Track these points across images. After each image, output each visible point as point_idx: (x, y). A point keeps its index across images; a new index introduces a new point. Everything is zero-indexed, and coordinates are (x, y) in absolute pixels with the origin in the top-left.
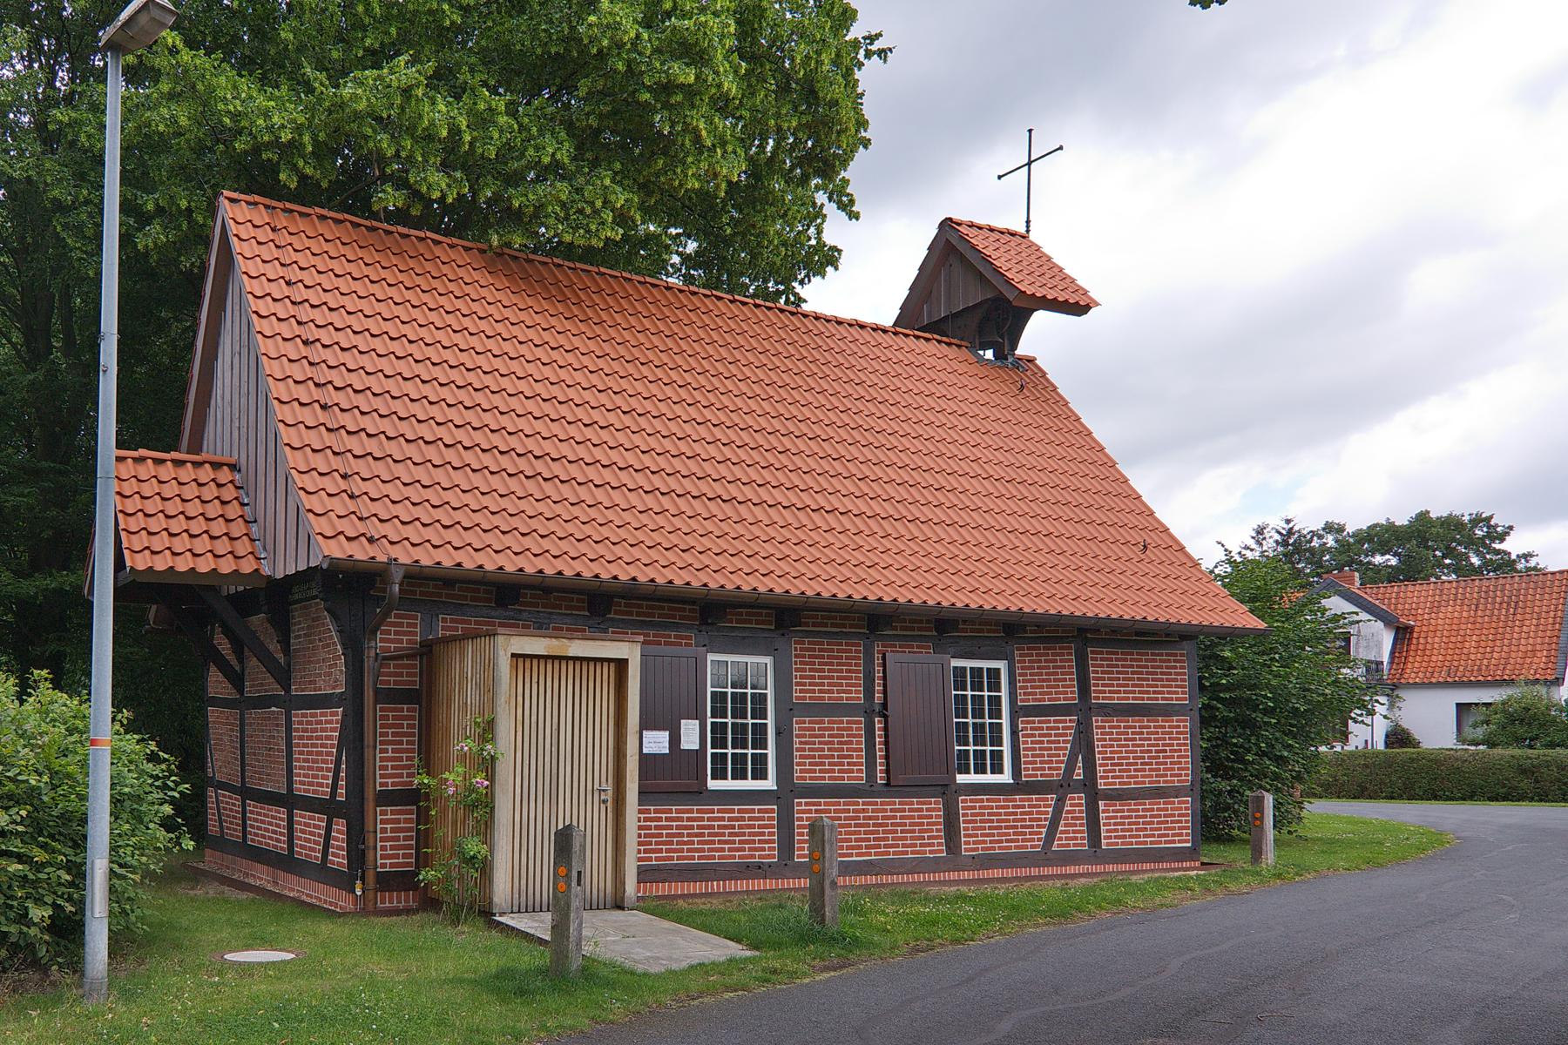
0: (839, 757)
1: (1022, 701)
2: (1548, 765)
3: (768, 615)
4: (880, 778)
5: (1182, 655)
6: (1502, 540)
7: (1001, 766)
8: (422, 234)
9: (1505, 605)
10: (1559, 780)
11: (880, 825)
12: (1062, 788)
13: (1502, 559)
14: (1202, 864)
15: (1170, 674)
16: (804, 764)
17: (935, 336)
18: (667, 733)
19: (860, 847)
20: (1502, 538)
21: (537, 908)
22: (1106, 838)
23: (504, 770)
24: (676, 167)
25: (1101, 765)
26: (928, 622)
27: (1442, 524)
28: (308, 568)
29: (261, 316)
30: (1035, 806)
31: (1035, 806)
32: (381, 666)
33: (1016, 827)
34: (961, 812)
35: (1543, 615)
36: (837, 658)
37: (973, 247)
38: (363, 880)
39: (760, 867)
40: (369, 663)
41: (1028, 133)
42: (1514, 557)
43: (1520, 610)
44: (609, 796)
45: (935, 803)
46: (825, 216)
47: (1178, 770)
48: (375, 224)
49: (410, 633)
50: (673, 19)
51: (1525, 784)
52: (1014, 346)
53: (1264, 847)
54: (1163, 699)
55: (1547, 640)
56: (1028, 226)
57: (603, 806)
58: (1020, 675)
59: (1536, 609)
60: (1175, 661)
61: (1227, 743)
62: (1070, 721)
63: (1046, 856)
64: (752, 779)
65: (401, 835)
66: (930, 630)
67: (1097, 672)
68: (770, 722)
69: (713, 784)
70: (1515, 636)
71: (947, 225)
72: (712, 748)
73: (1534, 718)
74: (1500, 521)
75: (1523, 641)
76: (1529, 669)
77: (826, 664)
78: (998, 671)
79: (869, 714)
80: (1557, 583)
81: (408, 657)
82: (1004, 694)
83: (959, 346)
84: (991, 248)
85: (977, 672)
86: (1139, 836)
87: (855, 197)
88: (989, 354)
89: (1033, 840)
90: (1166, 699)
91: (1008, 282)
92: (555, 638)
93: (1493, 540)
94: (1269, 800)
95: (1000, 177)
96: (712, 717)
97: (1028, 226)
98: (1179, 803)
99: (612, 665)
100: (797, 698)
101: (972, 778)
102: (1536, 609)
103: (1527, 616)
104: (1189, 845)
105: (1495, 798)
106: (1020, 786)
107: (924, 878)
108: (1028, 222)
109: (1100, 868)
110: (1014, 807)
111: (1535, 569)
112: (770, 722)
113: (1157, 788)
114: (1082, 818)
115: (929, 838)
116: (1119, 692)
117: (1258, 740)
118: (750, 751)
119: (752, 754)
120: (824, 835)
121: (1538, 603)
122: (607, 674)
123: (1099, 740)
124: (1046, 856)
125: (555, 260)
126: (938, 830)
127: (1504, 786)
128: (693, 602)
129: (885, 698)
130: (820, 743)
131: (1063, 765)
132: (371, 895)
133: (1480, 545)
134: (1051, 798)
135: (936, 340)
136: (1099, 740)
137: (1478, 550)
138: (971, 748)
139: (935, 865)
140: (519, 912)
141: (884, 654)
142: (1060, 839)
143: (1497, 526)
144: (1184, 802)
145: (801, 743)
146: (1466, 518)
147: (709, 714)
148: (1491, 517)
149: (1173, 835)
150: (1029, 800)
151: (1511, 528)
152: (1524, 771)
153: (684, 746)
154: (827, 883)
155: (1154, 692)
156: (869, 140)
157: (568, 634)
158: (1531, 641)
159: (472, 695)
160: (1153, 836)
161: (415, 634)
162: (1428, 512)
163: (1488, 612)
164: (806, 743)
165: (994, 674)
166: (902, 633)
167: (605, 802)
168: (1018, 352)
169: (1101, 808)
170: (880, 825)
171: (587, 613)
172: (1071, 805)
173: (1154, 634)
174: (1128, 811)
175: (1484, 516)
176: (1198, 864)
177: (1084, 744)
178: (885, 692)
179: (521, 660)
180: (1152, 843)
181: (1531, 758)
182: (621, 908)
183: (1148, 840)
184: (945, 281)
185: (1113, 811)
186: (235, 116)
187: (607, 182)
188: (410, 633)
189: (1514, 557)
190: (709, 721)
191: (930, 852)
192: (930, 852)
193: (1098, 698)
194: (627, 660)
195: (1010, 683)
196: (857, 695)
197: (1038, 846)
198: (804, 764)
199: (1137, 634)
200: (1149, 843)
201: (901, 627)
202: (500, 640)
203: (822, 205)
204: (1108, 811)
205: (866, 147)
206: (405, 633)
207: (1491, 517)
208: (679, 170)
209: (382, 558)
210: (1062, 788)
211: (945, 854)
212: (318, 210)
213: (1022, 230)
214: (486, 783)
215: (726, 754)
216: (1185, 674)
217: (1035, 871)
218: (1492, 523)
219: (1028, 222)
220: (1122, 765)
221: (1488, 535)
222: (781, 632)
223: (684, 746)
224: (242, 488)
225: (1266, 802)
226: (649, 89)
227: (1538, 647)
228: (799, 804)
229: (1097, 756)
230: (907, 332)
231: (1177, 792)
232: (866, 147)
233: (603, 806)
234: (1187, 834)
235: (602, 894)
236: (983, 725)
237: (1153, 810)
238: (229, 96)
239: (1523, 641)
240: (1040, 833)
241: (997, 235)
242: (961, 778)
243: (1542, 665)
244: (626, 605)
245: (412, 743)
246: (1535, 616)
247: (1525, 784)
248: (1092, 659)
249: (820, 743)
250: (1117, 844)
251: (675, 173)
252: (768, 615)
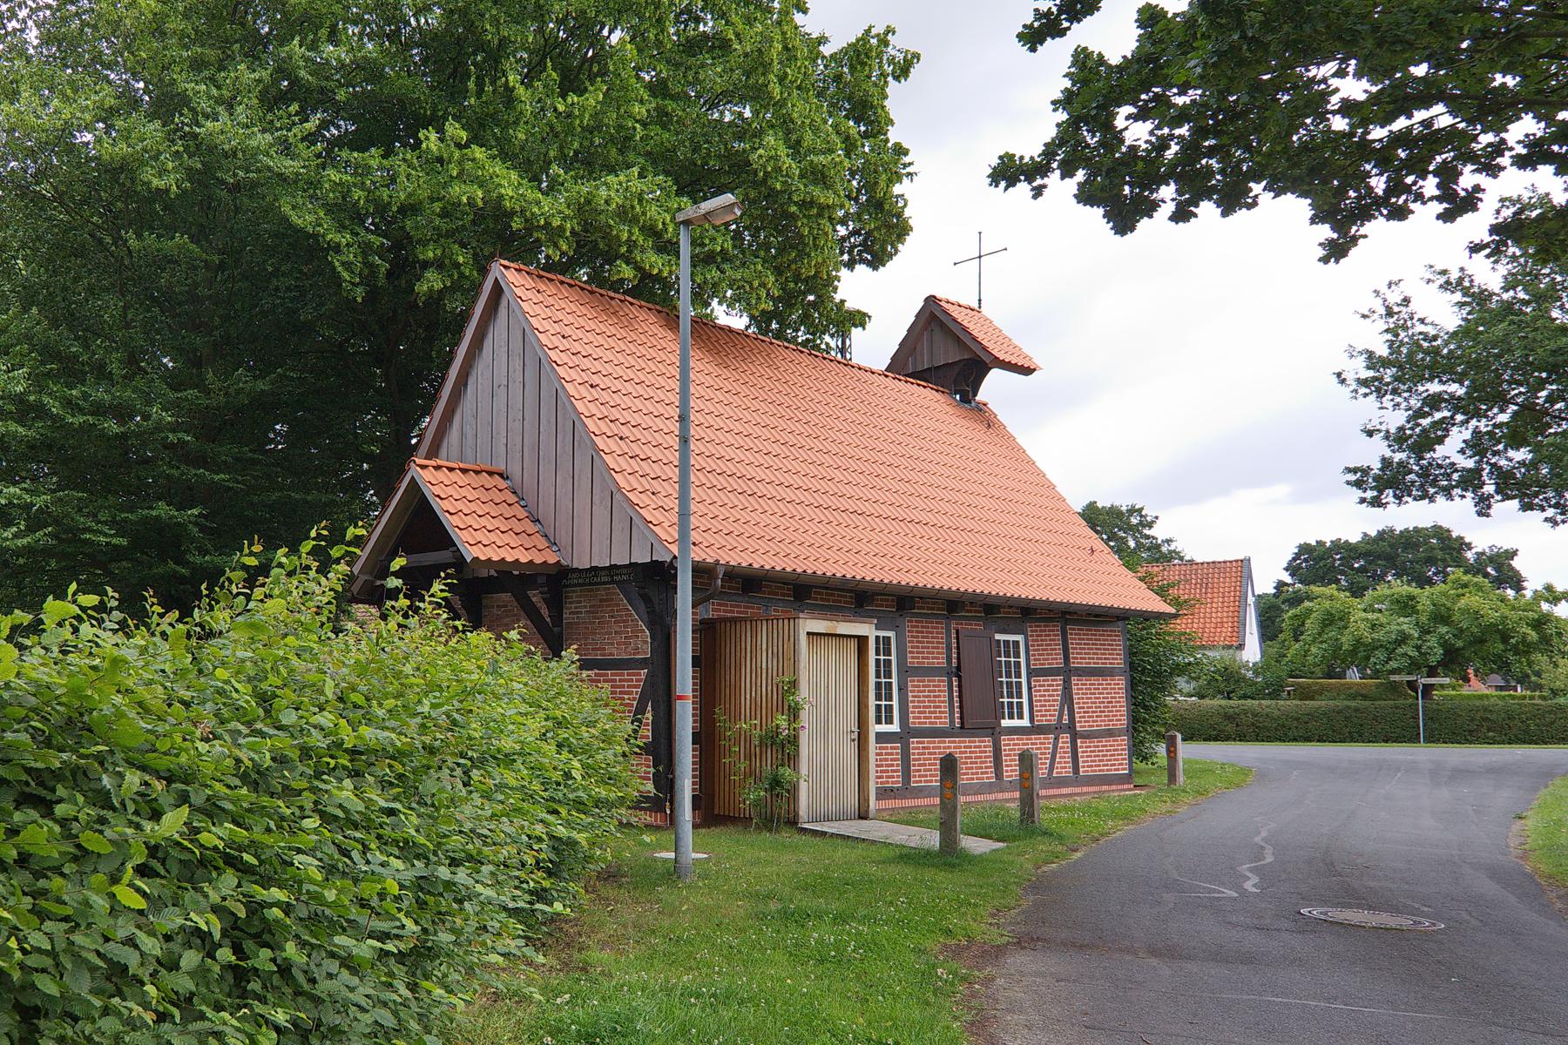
2: (1245, 712)
6: (1151, 527)
10: (1253, 724)
20: (1150, 525)
29: (558, 365)
42: (1159, 542)
43: (1209, 590)
44: (855, 736)
52: (975, 394)
55: (1230, 614)
56: (980, 304)
59: (1221, 590)
62: (1059, 680)
68: (894, 680)
74: (1149, 512)
75: (1214, 615)
76: (1220, 636)
83: (943, 392)
88: (958, 397)
97: (980, 304)
103: (1215, 595)
104: (1127, 772)
105: (1207, 739)
108: (980, 300)
111: (1174, 551)
113: (1109, 730)
121: (1222, 585)
122: (853, 645)
126: (990, 762)
146: (1124, 509)
148: (1142, 509)
151: (1157, 517)
152: (1229, 718)
158: (1219, 615)
162: (1095, 502)
163: (1187, 591)
167: (854, 740)
175: (1137, 507)
176: (1132, 786)
178: (958, 658)
182: (865, 818)
187: (759, 267)
189: (1159, 542)
196: (941, 661)
199: (1096, 616)
207: (1142, 509)
210: (1057, 729)
213: (976, 306)
218: (1143, 513)
219: (980, 300)
221: (1141, 523)
226: (796, 203)
227: (1225, 620)
230: (650, 306)
231: (1110, 733)
239: (1214, 615)
243: (1229, 634)
251: (803, 263)
252: (893, 601)
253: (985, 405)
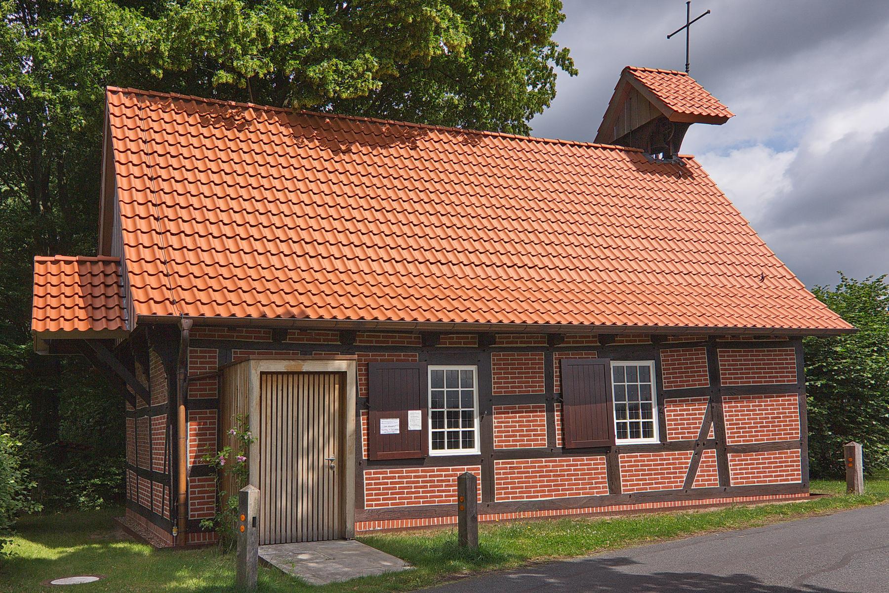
0: (527, 431)
4: (558, 444)
8: (402, 124)
11: (559, 476)
12: (699, 445)
14: (811, 495)
15: (783, 364)
16: (501, 437)
17: (618, 147)
18: (398, 420)
19: (544, 491)
21: (283, 540)
22: (733, 479)
23: (254, 449)
25: (728, 429)
26: (594, 337)
30: (677, 459)
31: (677, 459)
32: (189, 385)
33: (663, 474)
34: (620, 465)
36: (525, 364)
37: (644, 84)
38: (177, 525)
40: (180, 383)
45: (600, 459)
46: (556, 75)
48: (213, 100)
49: (211, 363)
52: (677, 148)
53: (856, 482)
54: (777, 381)
58: (664, 370)
60: (786, 355)
61: (843, 409)
63: (687, 493)
64: (448, 448)
65: (206, 495)
67: (725, 365)
69: (433, 453)
72: (433, 428)
77: (516, 369)
81: (210, 378)
84: (657, 84)
86: (760, 477)
87: (573, 60)
89: (676, 482)
90: (779, 381)
92: (293, 360)
94: (859, 448)
95: (669, 37)
96: (432, 408)
98: (791, 453)
99: (337, 376)
100: (495, 392)
101: (629, 441)
104: (800, 482)
106: (665, 446)
107: (593, 510)
109: (729, 500)
110: (661, 460)
114: (715, 466)
115: (596, 483)
116: (742, 378)
117: (866, 407)
119: (463, 431)
120: (466, 485)
123: (726, 412)
124: (687, 493)
125: (340, 115)
129: (561, 390)
130: (513, 422)
132: (182, 536)
134: (691, 453)
135: (618, 149)
136: (726, 412)
138: (628, 421)
139: (601, 501)
140: (270, 544)
141: (560, 360)
142: (698, 481)
144: (795, 452)
145: (498, 422)
147: (430, 405)
149: (787, 475)
150: (672, 455)
153: (411, 427)
155: (770, 377)
156: (564, 16)
157: (302, 357)
159: (240, 403)
160: (771, 476)
161: (215, 363)
164: (502, 422)
165: (645, 371)
166: (587, 345)
167: (332, 468)
168: (680, 154)
170: (559, 476)
172: (706, 457)
173: (768, 337)
174: (774, 458)
177: (716, 416)
180: (770, 481)
183: (767, 479)
185: (739, 460)
186: (121, 36)
188: (211, 363)
190: (430, 411)
191: (597, 493)
192: (597, 493)
195: (656, 376)
197: (681, 486)
198: (501, 437)
200: (768, 481)
201: (573, 341)
202: (252, 363)
203: (552, 68)
204: (735, 461)
205: (562, 20)
206: (207, 363)
209: (176, 314)
210: (699, 445)
212: (173, 94)
214: (244, 458)
215: (443, 432)
216: (794, 363)
217: (678, 504)
219: (687, 65)
220: (745, 428)
223: (411, 427)
224: (121, 276)
225: (856, 450)
228: (498, 464)
229: (725, 423)
231: (789, 445)
232: (562, 20)
234: (798, 475)
235: (331, 530)
237: (770, 458)
238: (115, 23)
240: (682, 477)
244: (247, 332)
245: (213, 434)
248: (721, 356)
249: (513, 422)
250: (743, 483)
253: (689, 159)
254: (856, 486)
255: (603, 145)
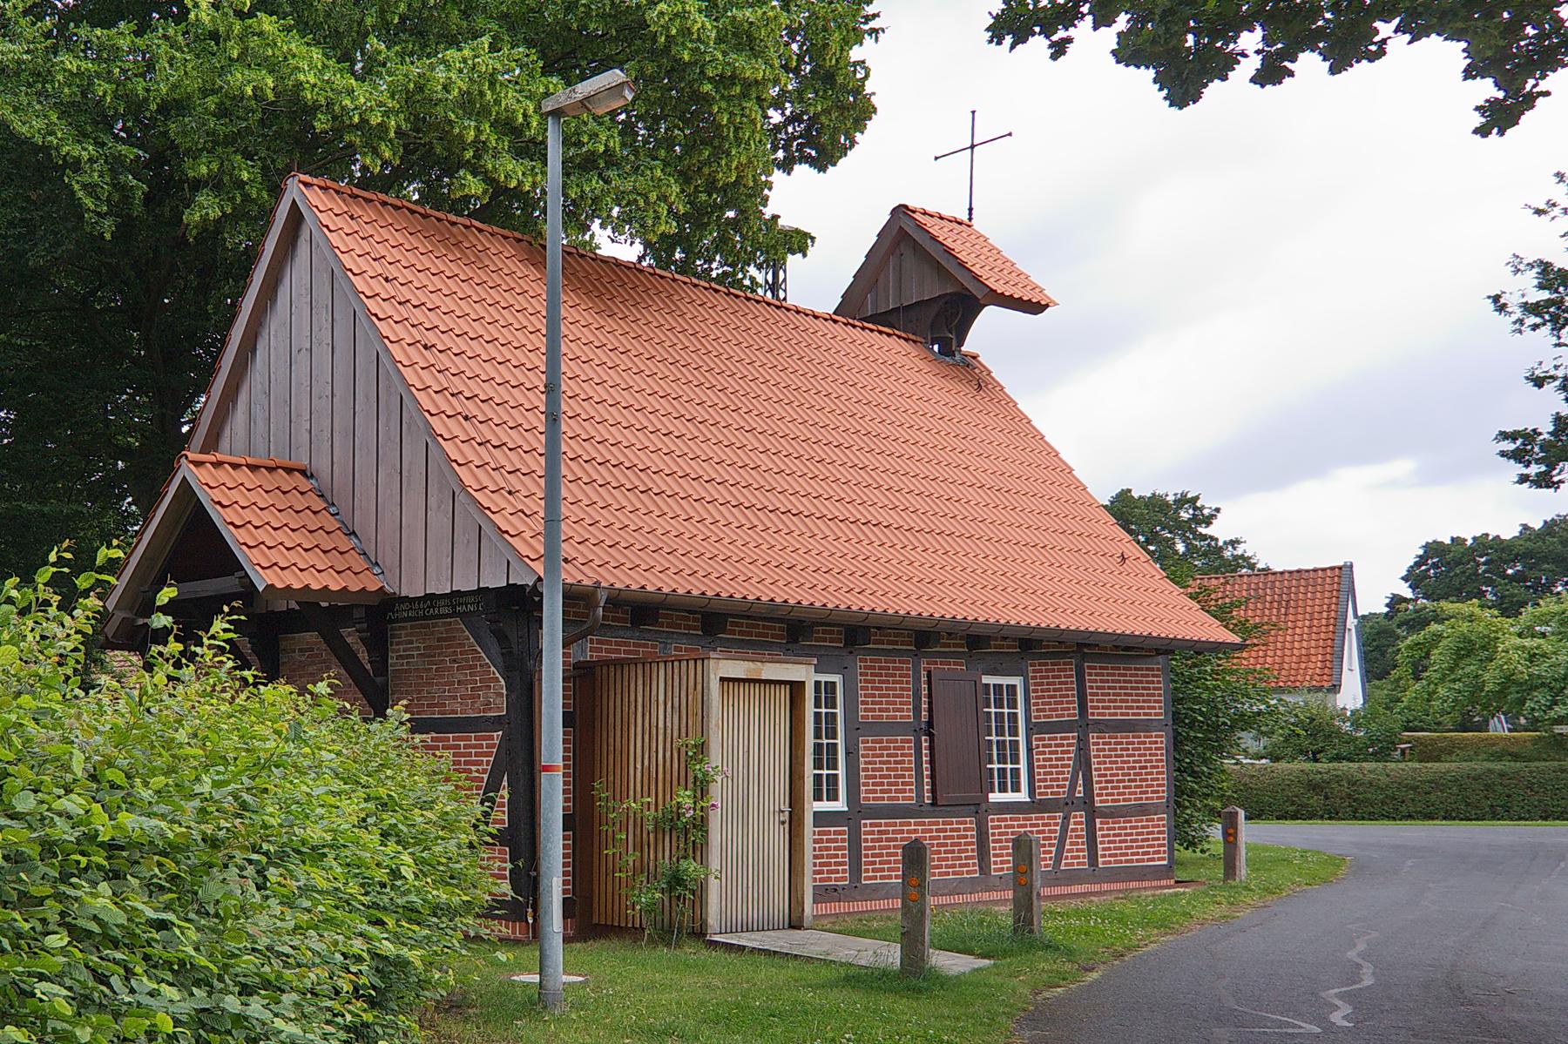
1: (1036, 717)
3: (839, 633)
5: (1158, 670)
6: (1208, 524)
7: (836, 791)
9: (1275, 604)
10: (1349, 796)
13: (1209, 545)
14: (1177, 882)
17: (897, 332)
20: (1208, 521)
24: (722, 158)
27: (1146, 506)
28: (479, 588)
35: (1316, 615)
39: (836, 890)
41: (971, 115)
43: (1291, 610)
44: (786, 817)
47: (896, 792)
50: (734, 9)
51: (1315, 801)
52: (961, 343)
53: (1238, 864)
56: (970, 214)
57: (782, 827)
59: (1309, 609)
66: (961, 646)
68: (840, 741)
70: (1288, 638)
71: (901, 211)
73: (1320, 728)
74: (1207, 503)
76: (1305, 675)
78: (1014, 687)
79: (917, 732)
80: (1328, 580)
82: (1020, 711)
83: (915, 342)
85: (998, 687)
88: (936, 348)
91: (976, 278)
93: (1199, 523)
97: (970, 214)
99: (788, 687)
102: (1309, 609)
103: (1300, 617)
104: (1165, 863)
108: (971, 209)
111: (1242, 557)
112: (840, 741)
113: (1141, 805)
118: (825, 772)
121: (1309, 602)
122: (784, 693)
127: (1293, 803)
128: (780, 620)
131: (1067, 783)
133: (1186, 529)
137: (1184, 535)
143: (1203, 507)
146: (1171, 498)
148: (1197, 498)
151: (1218, 510)
152: (1314, 787)
154: (1035, 894)
158: (1305, 644)
162: (1130, 491)
163: (1258, 612)
165: (1012, 688)
167: (783, 823)
169: (1098, 826)
171: (700, 633)
175: (1189, 496)
176: (1172, 882)
177: (1083, 762)
178: (930, 710)
179: (726, 683)
181: (1321, 773)
184: (894, 268)
187: (658, 173)
193: (1039, 717)
194: (804, 682)
196: (907, 714)
201: (740, 631)
207: (1197, 498)
208: (723, 162)
210: (1066, 805)
211: (978, 875)
213: (965, 218)
218: (1198, 504)
219: (971, 209)
222: (849, 650)
228: (865, 825)
231: (1143, 810)
233: (782, 827)
236: (1004, 741)
239: (1297, 645)
241: (945, 223)
242: (995, 797)
246: (1308, 616)
247: (1315, 801)
252: (839, 633)
254: (1238, 868)
255: (881, 328)
